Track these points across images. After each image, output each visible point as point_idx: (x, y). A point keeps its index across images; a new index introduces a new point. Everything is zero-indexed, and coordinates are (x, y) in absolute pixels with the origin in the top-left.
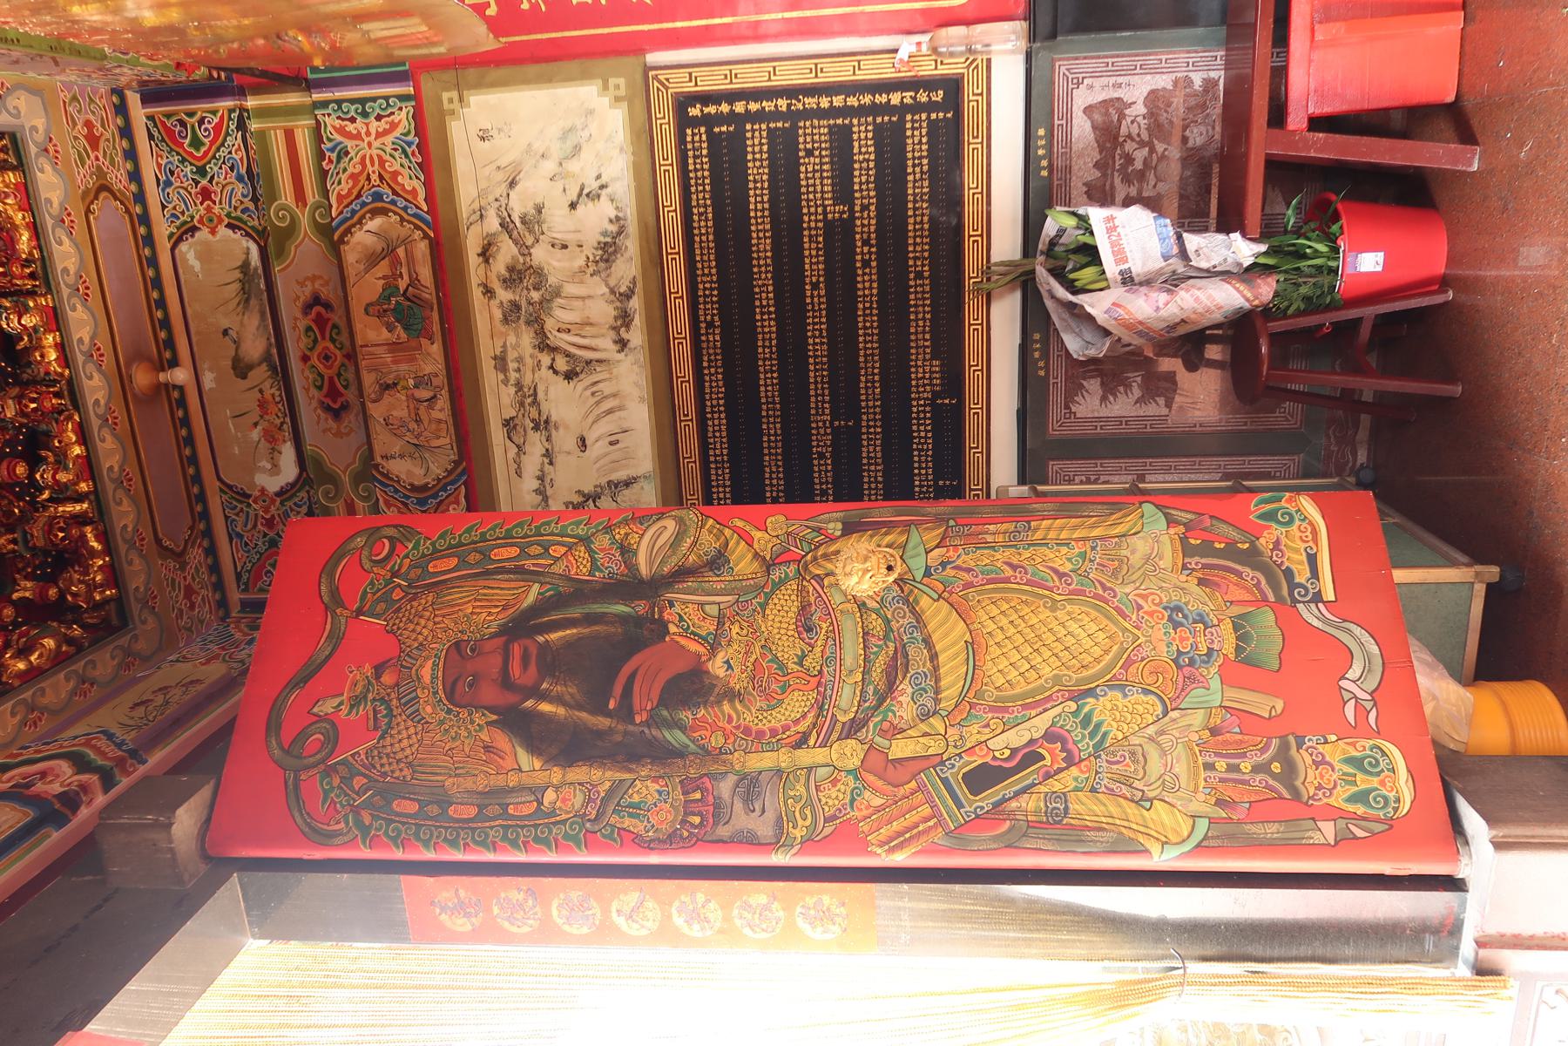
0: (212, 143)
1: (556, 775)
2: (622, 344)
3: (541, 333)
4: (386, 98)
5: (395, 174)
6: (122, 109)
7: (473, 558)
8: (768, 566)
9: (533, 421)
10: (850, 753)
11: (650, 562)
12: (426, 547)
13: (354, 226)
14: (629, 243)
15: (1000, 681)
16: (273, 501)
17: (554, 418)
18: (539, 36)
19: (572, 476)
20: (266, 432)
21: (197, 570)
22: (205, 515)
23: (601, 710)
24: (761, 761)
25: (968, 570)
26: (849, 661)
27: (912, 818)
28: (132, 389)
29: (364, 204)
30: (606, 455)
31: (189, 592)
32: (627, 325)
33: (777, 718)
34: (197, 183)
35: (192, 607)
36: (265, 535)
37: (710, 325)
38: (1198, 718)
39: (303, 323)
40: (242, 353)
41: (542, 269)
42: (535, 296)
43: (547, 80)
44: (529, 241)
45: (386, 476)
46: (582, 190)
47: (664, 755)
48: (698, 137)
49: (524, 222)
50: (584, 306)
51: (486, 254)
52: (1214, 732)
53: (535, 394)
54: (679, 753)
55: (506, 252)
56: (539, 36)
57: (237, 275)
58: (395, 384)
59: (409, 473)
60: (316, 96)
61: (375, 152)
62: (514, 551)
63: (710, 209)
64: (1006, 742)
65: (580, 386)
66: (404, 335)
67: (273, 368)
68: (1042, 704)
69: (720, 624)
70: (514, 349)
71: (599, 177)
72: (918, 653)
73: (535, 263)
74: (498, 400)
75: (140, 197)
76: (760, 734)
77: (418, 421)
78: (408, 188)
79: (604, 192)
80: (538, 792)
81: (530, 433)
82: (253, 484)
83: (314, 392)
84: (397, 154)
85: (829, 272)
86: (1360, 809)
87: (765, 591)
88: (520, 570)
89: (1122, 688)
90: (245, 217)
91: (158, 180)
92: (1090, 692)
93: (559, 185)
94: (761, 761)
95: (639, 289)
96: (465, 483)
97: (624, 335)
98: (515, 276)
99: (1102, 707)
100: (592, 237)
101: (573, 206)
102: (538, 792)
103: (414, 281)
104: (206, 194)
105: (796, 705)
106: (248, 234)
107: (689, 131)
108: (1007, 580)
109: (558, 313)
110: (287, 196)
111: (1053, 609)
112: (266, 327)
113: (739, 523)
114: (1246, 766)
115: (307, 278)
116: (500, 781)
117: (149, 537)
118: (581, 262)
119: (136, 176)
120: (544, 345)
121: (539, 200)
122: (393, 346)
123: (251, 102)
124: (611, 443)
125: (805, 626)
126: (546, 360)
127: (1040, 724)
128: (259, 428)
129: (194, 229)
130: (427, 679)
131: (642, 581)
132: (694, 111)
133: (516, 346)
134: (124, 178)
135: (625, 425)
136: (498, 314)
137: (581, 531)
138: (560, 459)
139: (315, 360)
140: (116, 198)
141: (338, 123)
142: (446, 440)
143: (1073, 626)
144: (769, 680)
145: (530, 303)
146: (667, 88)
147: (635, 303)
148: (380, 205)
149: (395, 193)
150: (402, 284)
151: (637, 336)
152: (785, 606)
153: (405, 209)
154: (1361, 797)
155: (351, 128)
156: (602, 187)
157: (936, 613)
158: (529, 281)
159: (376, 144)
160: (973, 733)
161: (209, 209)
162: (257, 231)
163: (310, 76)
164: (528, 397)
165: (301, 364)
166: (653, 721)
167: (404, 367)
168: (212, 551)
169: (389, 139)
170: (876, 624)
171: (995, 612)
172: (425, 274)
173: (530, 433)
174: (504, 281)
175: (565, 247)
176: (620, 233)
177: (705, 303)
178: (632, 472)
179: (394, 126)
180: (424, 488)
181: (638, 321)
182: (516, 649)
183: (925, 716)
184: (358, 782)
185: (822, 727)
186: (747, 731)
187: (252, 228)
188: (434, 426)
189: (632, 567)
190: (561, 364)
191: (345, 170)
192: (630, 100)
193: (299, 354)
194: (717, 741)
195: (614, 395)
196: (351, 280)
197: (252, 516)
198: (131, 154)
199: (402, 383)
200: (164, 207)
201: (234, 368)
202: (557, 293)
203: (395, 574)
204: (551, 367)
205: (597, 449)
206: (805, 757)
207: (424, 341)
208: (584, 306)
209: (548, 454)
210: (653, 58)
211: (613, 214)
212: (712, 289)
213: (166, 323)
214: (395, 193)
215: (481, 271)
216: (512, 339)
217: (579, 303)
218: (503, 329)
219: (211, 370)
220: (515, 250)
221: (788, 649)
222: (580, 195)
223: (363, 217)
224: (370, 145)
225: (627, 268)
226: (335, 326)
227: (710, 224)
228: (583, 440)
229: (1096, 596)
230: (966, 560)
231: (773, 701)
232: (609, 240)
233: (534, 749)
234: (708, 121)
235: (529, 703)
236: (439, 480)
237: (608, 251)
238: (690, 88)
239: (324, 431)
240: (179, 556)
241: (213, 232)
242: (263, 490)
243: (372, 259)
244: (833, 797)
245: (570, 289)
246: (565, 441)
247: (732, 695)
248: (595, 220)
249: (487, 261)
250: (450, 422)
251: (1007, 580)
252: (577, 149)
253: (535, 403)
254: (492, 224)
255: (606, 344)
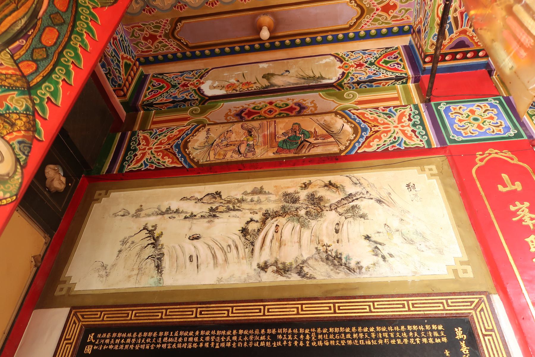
0: (388, 67)
2: (264, 267)
3: (276, 215)
4: (426, 134)
5: (380, 138)
6: (401, 32)
9: (217, 208)
13: (346, 119)
16: (196, 87)
17: (216, 220)
18: (492, 216)
19: (173, 232)
20: (234, 84)
21: (165, 46)
22: (194, 57)
28: (259, 15)
29: (360, 124)
30: (183, 253)
31: (153, 38)
34: (366, 62)
35: (145, 39)
36: (179, 84)
37: (274, 338)
39: (290, 103)
40: (275, 77)
41: (321, 216)
42: (302, 212)
43: (459, 224)
44: (340, 210)
45: (198, 130)
46: (380, 244)
48: (436, 336)
49: (353, 207)
50: (295, 243)
51: (330, 185)
53: (234, 210)
56: (492, 216)
57: (318, 75)
58: (251, 135)
59: (197, 140)
60: (422, 106)
61: (392, 129)
63: (374, 343)
65: (236, 238)
66: (280, 140)
67: (267, 87)
70: (267, 199)
71: (391, 255)
73: (325, 212)
74: (232, 189)
75: (357, 37)
77: (227, 145)
78: (371, 144)
79: (380, 259)
82: (207, 79)
83: (252, 106)
84: (392, 139)
90: (349, 78)
91: (366, 50)
93: (382, 229)
95: (305, 281)
96: (183, 167)
97: (270, 269)
98: (315, 201)
100: (345, 250)
101: (367, 238)
104: (360, 65)
106: (339, 79)
107: (440, 327)
109: (290, 226)
110: (360, 97)
112: (290, 85)
115: (315, 104)
117: (184, 13)
118: (326, 241)
119: (368, 36)
121: (369, 216)
122: (274, 135)
123: (411, 85)
124: (191, 257)
126: (258, 217)
128: (236, 82)
129: (341, 61)
132: (459, 333)
133: (268, 200)
134: (367, 27)
135: (202, 267)
136: (290, 191)
138: (188, 223)
139: (269, 107)
140: (358, 19)
141: (407, 114)
142: (212, 158)
145: (297, 209)
146: (475, 309)
147: (294, 278)
148: (360, 130)
149: (367, 138)
150: (312, 140)
151: (269, 278)
153: (358, 142)
155: (405, 119)
156: (384, 258)
158: (311, 208)
159: (397, 130)
161: (352, 66)
162: (341, 82)
163: (432, 103)
164: (233, 206)
165: (268, 101)
167: (261, 139)
168: (175, 59)
169: (401, 135)
172: (318, 151)
173: (209, 206)
174: (312, 195)
175: (337, 231)
176: (349, 269)
177: (293, 334)
178: (166, 271)
179: (410, 138)
180: (186, 146)
181: (280, 279)
187: (343, 81)
188: (222, 153)
190: (253, 227)
191: (379, 116)
192: (457, 280)
193: (274, 101)
195: (226, 260)
196: (314, 118)
197: (190, 79)
198: (379, 35)
199: (251, 139)
200: (352, 52)
201: (268, 74)
202: (303, 225)
204: (252, 220)
205: (189, 247)
207: (275, 149)
208: (295, 243)
209: (193, 216)
210: (497, 300)
211: (364, 264)
212: (305, 341)
213: (293, 45)
214: (367, 138)
215: (319, 182)
216: (273, 198)
217: (296, 238)
218: (281, 193)
219: (268, 66)
220: (334, 201)
222: (376, 242)
223: (351, 123)
224: (396, 127)
225: (322, 274)
227: (362, 342)
228: (197, 238)
232: (344, 261)
234: (453, 344)
236: (189, 154)
237: (335, 260)
238: (480, 329)
239: (230, 110)
240: (171, 34)
241: (340, 67)
242: (203, 83)
243: (327, 127)
245: (306, 234)
246: (199, 227)
248: (357, 251)
249: (326, 186)
250: (223, 161)
252: (411, 242)
253: (229, 210)
254: (351, 189)
255: (265, 256)
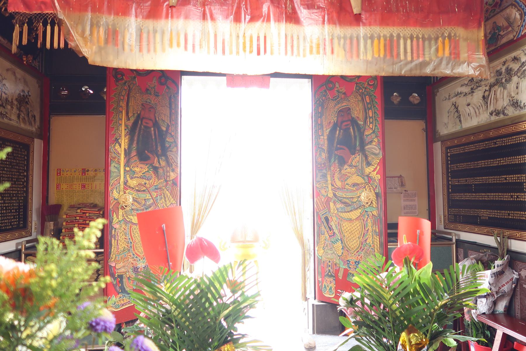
1: (326, 138)
2: (491, 114)
7: (369, 106)
8: (368, 176)
10: (331, 195)
11: (368, 148)
12: (372, 93)
14: (518, 111)
15: (344, 225)
17: (474, 94)
23: (337, 144)
24: (329, 178)
25: (367, 220)
26: (347, 194)
27: (320, 206)
32: (496, 115)
33: (337, 180)
38: (338, 262)
42: (504, 80)
47: (329, 158)
52: (336, 264)
53: (479, 86)
54: (330, 161)
55: (515, 66)
62: (371, 115)
64: (332, 224)
65: (481, 101)
68: (339, 232)
69: (355, 166)
72: (349, 208)
76: (333, 177)
80: (323, 135)
81: (470, 87)
85: (509, 183)
86: (323, 286)
87: (362, 174)
88: (366, 118)
89: (343, 249)
92: (342, 243)
94: (329, 178)
95: (506, 117)
97: (493, 114)
98: (509, 71)
99: (339, 244)
102: (323, 135)
103: (503, 37)
105: (339, 184)
108: (365, 229)
111: (358, 238)
113: (378, 168)
114: (330, 268)
116: (324, 127)
118: (513, 95)
120: (491, 86)
125: (354, 185)
126: (487, 88)
127: (336, 232)
130: (343, 105)
131: (364, 147)
136: (498, 68)
137: (376, 130)
143: (355, 241)
144: (344, 178)
151: (494, 118)
152: (359, 180)
153: (522, 26)
154: (325, 287)
157: (358, 213)
160: (334, 219)
166: (335, 155)
170: (355, 200)
171: (358, 225)
172: (504, 40)
173: (470, 87)
174: (507, 68)
175: (517, 88)
182: (349, 122)
183: (337, 209)
184: (324, 98)
185: (335, 189)
186: (334, 174)
189: (367, 144)
194: (332, 168)
195: (479, 113)
202: (505, 88)
203: (365, 88)
204: (486, 90)
206: (330, 186)
217: (502, 97)
220: (516, 70)
221: (350, 181)
225: (511, 112)
226: (495, 10)
229: (361, 247)
230: (369, 221)
231: (339, 179)
233: (330, 132)
235: (338, 128)
244: (323, 191)
245: (506, 92)
246: (469, 99)
247: (340, 170)
251: (365, 229)
253: (477, 87)
255: (491, 108)
